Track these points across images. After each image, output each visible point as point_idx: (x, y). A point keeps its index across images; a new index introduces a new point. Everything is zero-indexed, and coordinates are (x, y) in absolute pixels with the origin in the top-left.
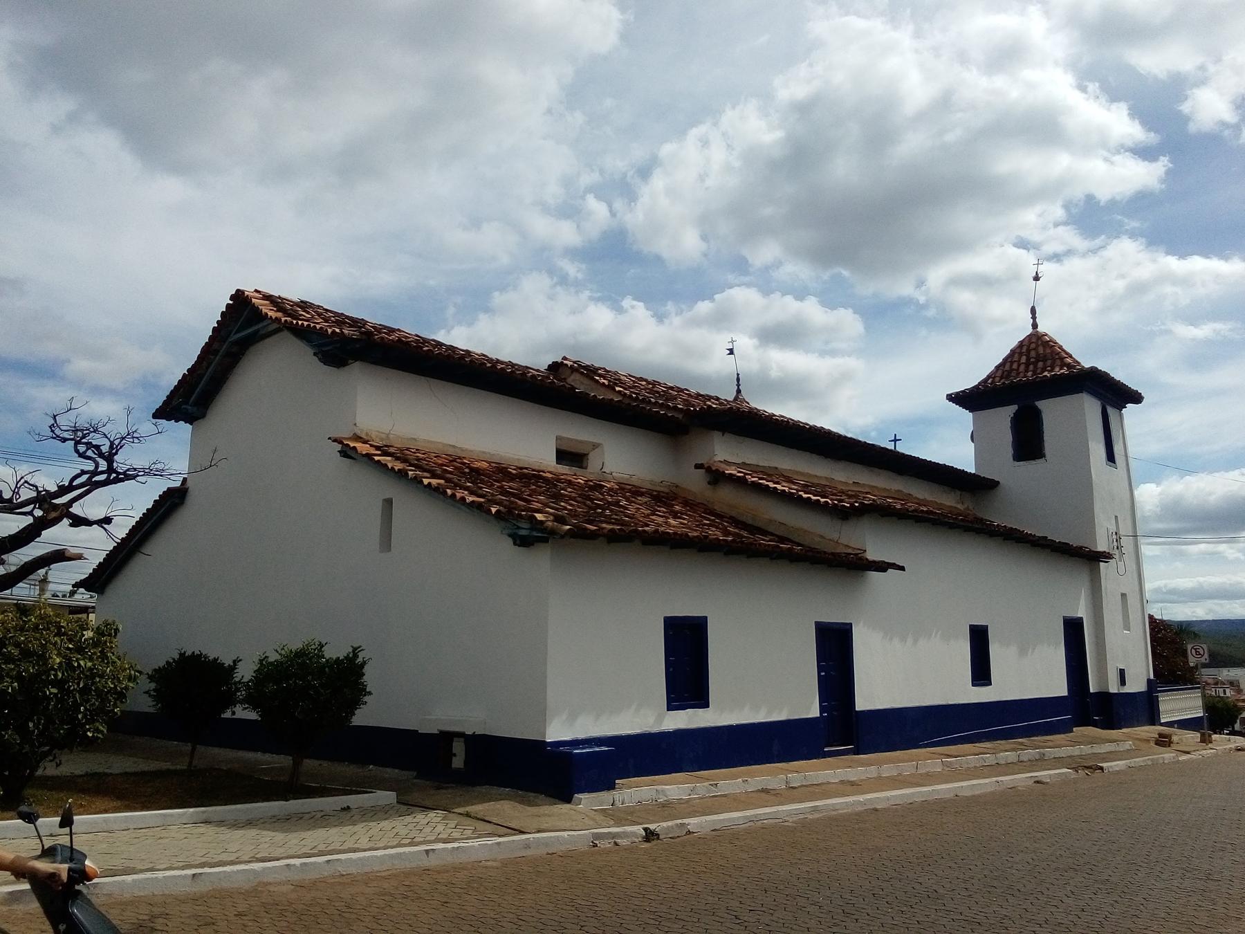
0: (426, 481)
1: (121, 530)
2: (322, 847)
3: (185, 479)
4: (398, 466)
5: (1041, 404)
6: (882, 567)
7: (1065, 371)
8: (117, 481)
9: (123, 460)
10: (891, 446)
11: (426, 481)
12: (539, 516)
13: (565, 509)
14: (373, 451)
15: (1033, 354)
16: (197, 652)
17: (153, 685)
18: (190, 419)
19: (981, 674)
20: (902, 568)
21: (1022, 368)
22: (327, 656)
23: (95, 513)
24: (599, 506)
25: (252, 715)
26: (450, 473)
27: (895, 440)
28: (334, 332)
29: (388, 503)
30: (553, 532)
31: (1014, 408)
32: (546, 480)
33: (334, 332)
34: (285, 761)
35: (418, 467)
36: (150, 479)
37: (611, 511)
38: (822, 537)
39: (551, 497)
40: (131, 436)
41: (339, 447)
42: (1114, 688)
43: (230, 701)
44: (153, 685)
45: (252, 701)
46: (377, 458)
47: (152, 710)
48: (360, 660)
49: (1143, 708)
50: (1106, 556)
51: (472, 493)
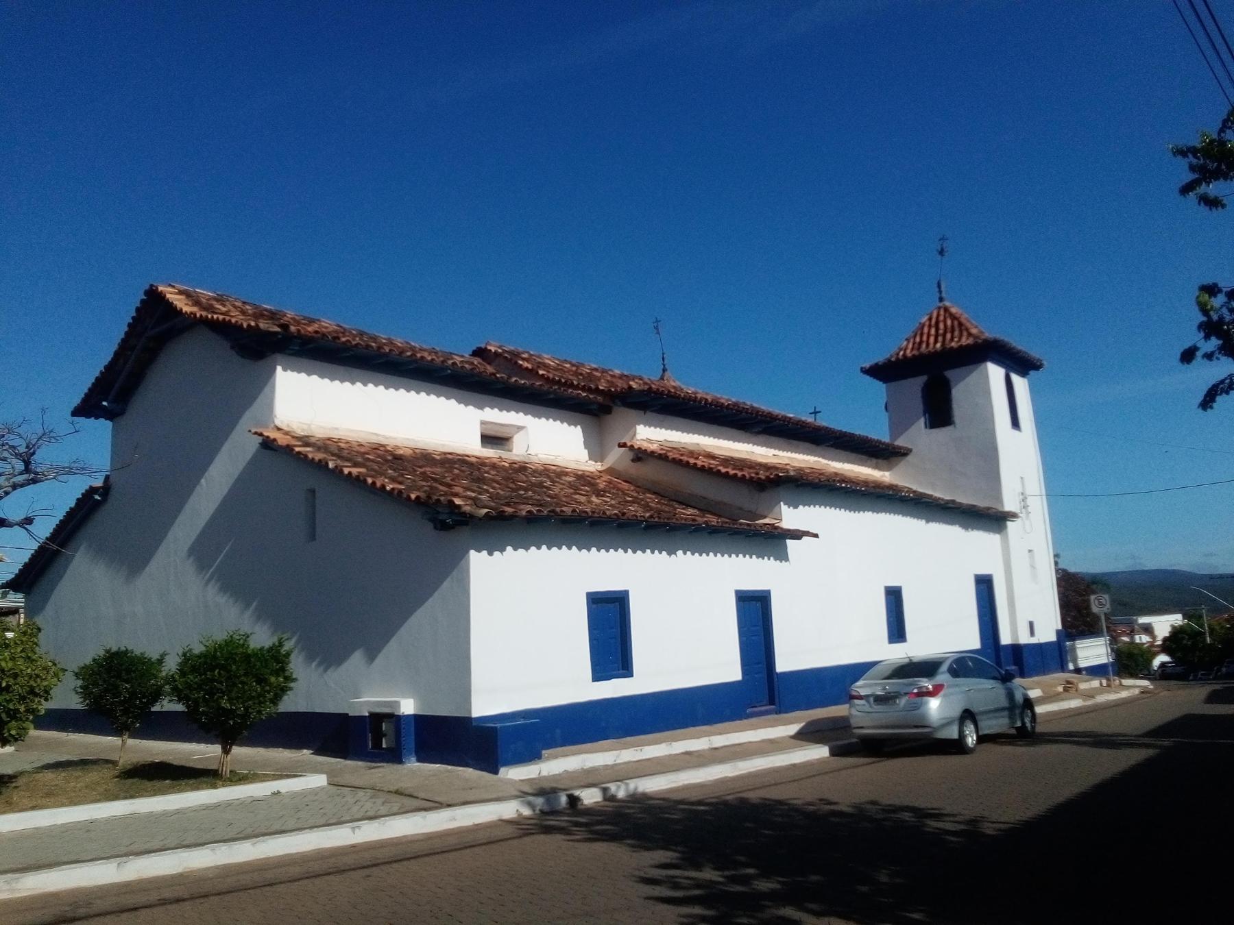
0: (346, 471)
1: (44, 528)
2: (249, 831)
3: (107, 478)
4: (319, 456)
5: (949, 374)
6: (797, 535)
7: (970, 341)
8: (34, 481)
9: (44, 457)
10: (810, 419)
11: (346, 471)
12: (458, 501)
13: (487, 491)
14: (294, 442)
15: (941, 326)
16: (123, 649)
17: (80, 683)
18: (110, 415)
19: (897, 632)
20: (816, 536)
21: (932, 340)
22: (252, 646)
23: (15, 516)
24: (522, 488)
25: (180, 707)
26: (372, 461)
27: (815, 413)
28: (249, 325)
29: (313, 492)
30: (472, 516)
31: (924, 378)
32: (471, 464)
33: (249, 325)
34: (215, 750)
35: (340, 457)
36: (71, 477)
37: (534, 492)
38: (740, 509)
39: (473, 480)
40: (47, 435)
41: (260, 439)
42: (1024, 639)
43: (156, 696)
44: (80, 683)
45: (180, 696)
46: (297, 449)
47: (79, 707)
48: (283, 651)
49: (1052, 657)
50: (1013, 516)
51: (393, 480)
